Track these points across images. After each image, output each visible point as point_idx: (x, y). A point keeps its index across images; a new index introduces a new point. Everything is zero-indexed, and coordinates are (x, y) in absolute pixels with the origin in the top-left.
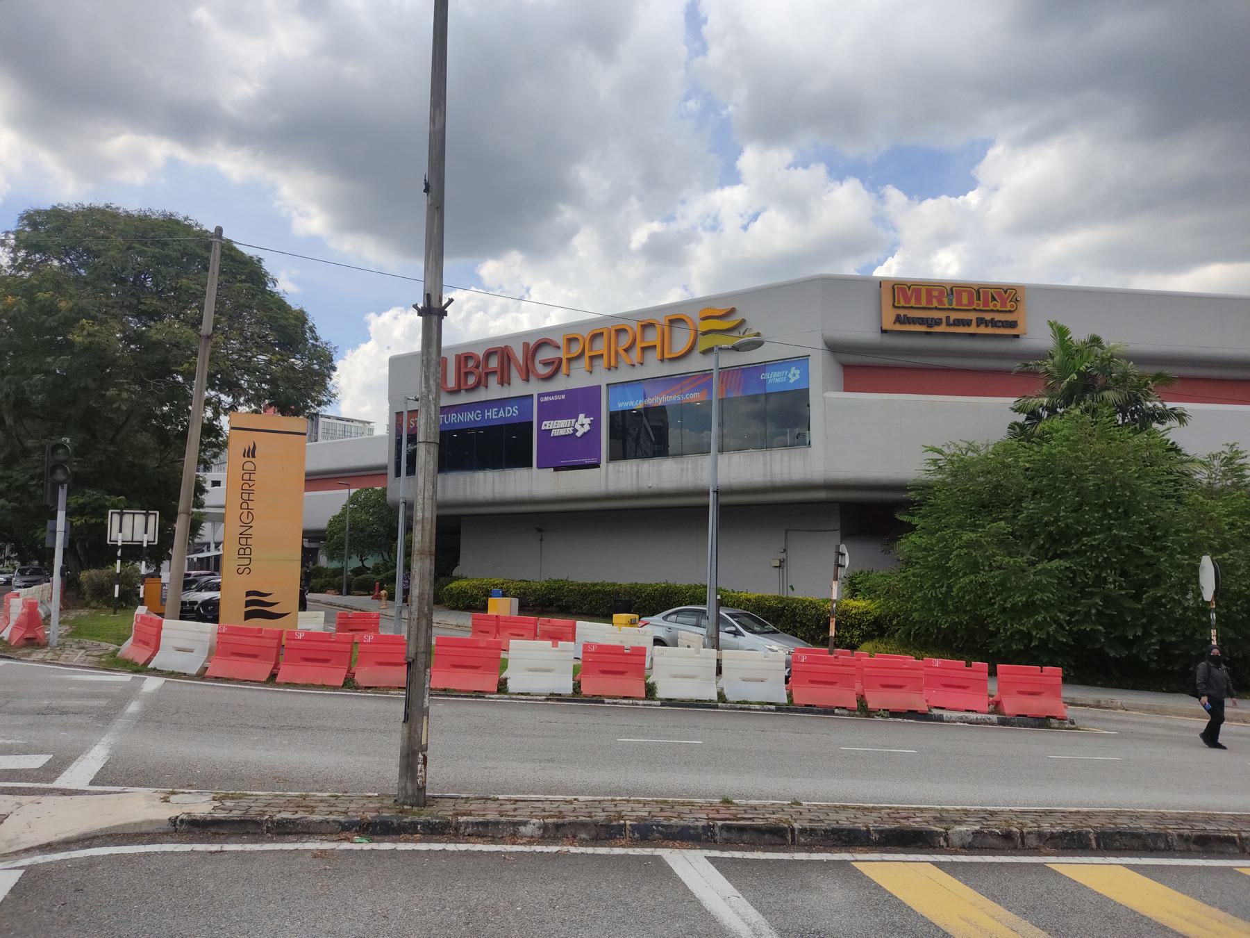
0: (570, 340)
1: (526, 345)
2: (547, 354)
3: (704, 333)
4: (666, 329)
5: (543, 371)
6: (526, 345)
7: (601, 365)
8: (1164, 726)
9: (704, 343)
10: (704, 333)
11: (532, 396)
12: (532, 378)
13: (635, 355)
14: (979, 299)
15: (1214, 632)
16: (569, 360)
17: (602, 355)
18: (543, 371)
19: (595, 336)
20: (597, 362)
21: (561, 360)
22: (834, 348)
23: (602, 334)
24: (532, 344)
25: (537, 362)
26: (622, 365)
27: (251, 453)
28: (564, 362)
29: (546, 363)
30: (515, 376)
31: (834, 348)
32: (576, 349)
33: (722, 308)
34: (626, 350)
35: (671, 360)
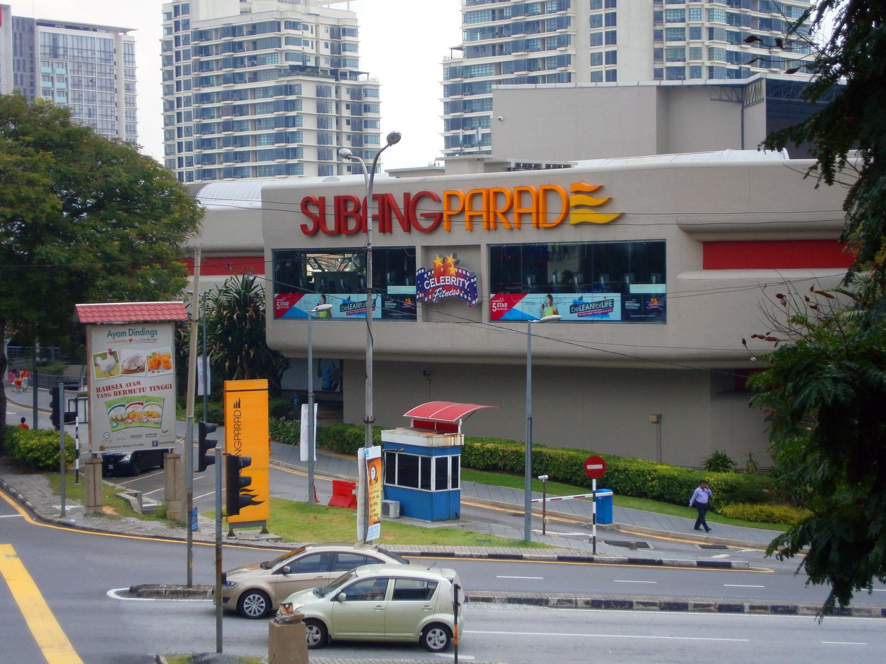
0: (450, 197)
1: (407, 196)
2: (427, 206)
3: (577, 207)
4: (541, 195)
5: (426, 224)
6: (407, 196)
7: (480, 226)
8: (632, 535)
9: (576, 217)
10: (577, 207)
11: (478, 247)
12: (413, 229)
13: (513, 218)
14: (424, 592)
15: (38, 351)
16: (450, 216)
17: (531, 214)
18: (426, 224)
19: (474, 196)
20: (526, 220)
21: (441, 215)
22: (690, 231)
23: (481, 194)
24: (412, 197)
25: (418, 214)
26: (501, 227)
27: (238, 405)
28: (445, 218)
29: (427, 216)
30: (396, 224)
31: (690, 231)
32: (457, 206)
33: (589, 185)
34: (504, 214)
35: (546, 228)
